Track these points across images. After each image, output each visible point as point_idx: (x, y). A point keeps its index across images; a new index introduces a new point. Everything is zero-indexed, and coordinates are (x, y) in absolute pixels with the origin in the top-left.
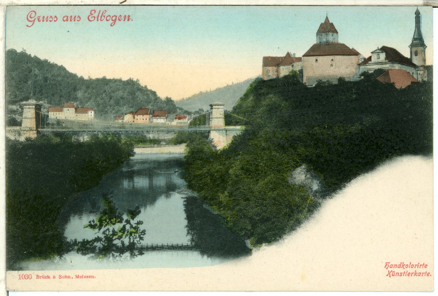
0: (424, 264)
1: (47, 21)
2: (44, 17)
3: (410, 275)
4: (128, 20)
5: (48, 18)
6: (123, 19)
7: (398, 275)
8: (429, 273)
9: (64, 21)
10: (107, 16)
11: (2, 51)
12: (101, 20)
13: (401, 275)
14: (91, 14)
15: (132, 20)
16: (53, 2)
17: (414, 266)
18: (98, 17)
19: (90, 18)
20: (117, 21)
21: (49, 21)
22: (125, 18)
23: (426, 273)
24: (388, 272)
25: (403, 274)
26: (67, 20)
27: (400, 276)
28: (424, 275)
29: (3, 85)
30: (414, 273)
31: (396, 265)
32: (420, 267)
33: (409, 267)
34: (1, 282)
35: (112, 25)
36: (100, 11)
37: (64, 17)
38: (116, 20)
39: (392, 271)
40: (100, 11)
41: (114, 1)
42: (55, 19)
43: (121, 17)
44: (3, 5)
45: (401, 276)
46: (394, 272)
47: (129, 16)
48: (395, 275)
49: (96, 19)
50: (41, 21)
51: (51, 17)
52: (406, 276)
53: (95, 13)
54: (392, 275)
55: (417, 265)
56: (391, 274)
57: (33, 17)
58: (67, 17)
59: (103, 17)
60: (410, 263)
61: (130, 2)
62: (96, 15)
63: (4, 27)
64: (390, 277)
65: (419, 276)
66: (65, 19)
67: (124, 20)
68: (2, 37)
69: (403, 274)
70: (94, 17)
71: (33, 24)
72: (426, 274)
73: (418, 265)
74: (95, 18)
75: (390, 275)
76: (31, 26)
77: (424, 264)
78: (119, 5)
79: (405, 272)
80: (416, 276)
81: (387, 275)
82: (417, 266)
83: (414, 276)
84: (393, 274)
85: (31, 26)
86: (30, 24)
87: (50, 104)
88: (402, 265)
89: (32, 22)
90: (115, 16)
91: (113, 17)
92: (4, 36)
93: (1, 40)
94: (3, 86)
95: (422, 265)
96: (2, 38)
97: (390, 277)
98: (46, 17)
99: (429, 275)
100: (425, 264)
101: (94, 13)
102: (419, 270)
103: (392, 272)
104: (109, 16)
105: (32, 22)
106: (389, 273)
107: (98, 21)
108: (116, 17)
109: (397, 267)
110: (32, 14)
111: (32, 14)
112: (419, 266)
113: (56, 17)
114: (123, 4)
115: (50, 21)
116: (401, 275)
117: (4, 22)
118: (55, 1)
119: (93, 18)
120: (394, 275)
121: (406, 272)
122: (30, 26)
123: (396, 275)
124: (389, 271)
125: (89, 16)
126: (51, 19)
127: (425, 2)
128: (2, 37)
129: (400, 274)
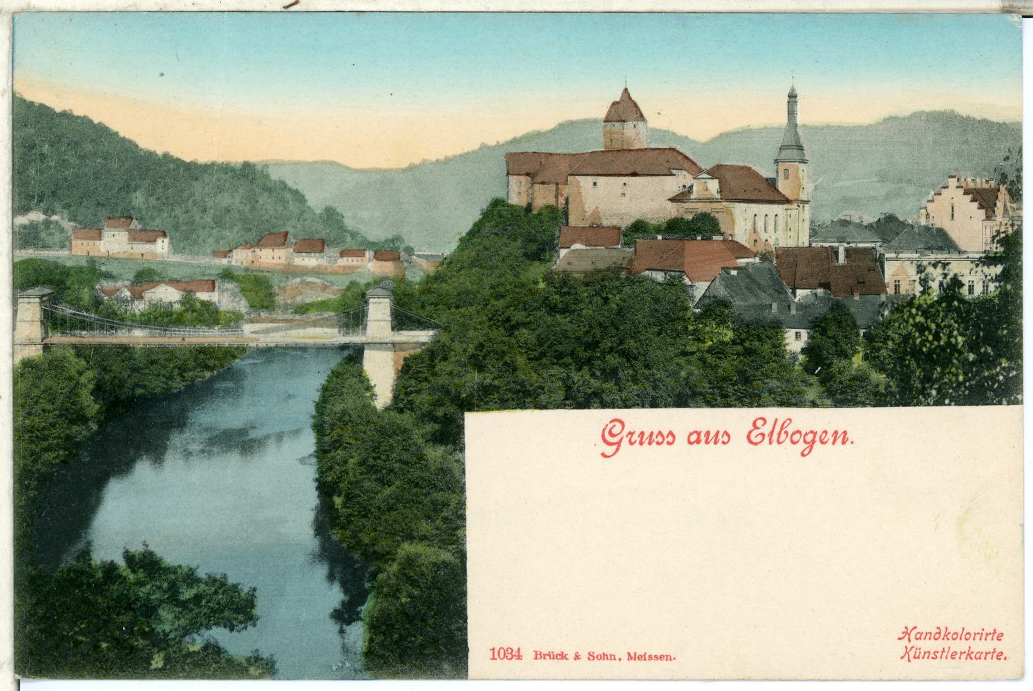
0: (995, 630)
1: (650, 443)
2: (642, 433)
3: (957, 657)
4: (844, 442)
5: (654, 437)
6: (832, 439)
7: (928, 658)
8: (1002, 653)
9: (690, 443)
10: (794, 434)
11: (6, 121)
12: (779, 442)
13: (935, 657)
14: (756, 427)
15: (852, 443)
16: (126, 5)
17: (973, 635)
18: (772, 435)
19: (752, 437)
20: (817, 444)
21: (654, 444)
22: (835, 437)
23: (993, 652)
24: (904, 651)
25: (939, 655)
26: (698, 441)
27: (933, 658)
28: (989, 656)
29: (7, 201)
30: (967, 652)
31: (931, 633)
32: (986, 639)
33: (961, 639)
34: (1, 668)
35: (806, 452)
36: (776, 420)
37: (691, 434)
38: (813, 441)
39: (913, 647)
40: (776, 420)
41: (270, 3)
42: (670, 439)
43: (826, 435)
44: (8, 13)
45: (935, 652)
46: (920, 649)
47: (845, 433)
48: (921, 656)
49: (767, 439)
50: (637, 444)
51: (660, 433)
52: (946, 658)
53: (766, 426)
54: (915, 658)
55: (979, 633)
56: (912, 654)
57: (618, 434)
58: (699, 434)
59: (783, 436)
60: (963, 629)
61: (308, 4)
62: (767, 429)
63: (9, 64)
64: (909, 661)
65: (979, 660)
66: (694, 438)
67: (834, 443)
68: (6, 88)
69: (939, 655)
70: (763, 435)
71: (617, 450)
72: (996, 635)
73: (982, 634)
74: (763, 439)
75: (909, 655)
76: (612, 455)
77: (995, 630)
78: (281, 12)
79: (944, 651)
80: (971, 658)
81: (902, 658)
82: (978, 637)
83: (966, 659)
84: (917, 655)
85: (612, 455)
86: (610, 450)
87: (75, 221)
88: (941, 634)
89: (615, 447)
90: (812, 432)
91: (806, 434)
92: (10, 84)
93: (3, 95)
94: (8, 203)
95: (990, 634)
96: (4, 91)
97: (909, 661)
98: (647, 434)
99: (1002, 657)
100: (998, 632)
101: (763, 425)
102: (978, 646)
103: (914, 650)
104: (798, 432)
105: (615, 447)
106: (907, 652)
107: (770, 443)
108: (815, 434)
109: (932, 638)
110: (615, 426)
111: (615, 426)
112: (984, 636)
113: (671, 433)
114: (292, 9)
115: (658, 443)
116: (935, 657)
117: (9, 51)
118: (130, 3)
119: (760, 438)
120: (918, 658)
121: (946, 650)
122: (610, 454)
123: (923, 658)
124: (906, 647)
125: (750, 432)
126: (660, 439)
127: (1007, 4)
128: (6, 88)
129: (932, 655)
